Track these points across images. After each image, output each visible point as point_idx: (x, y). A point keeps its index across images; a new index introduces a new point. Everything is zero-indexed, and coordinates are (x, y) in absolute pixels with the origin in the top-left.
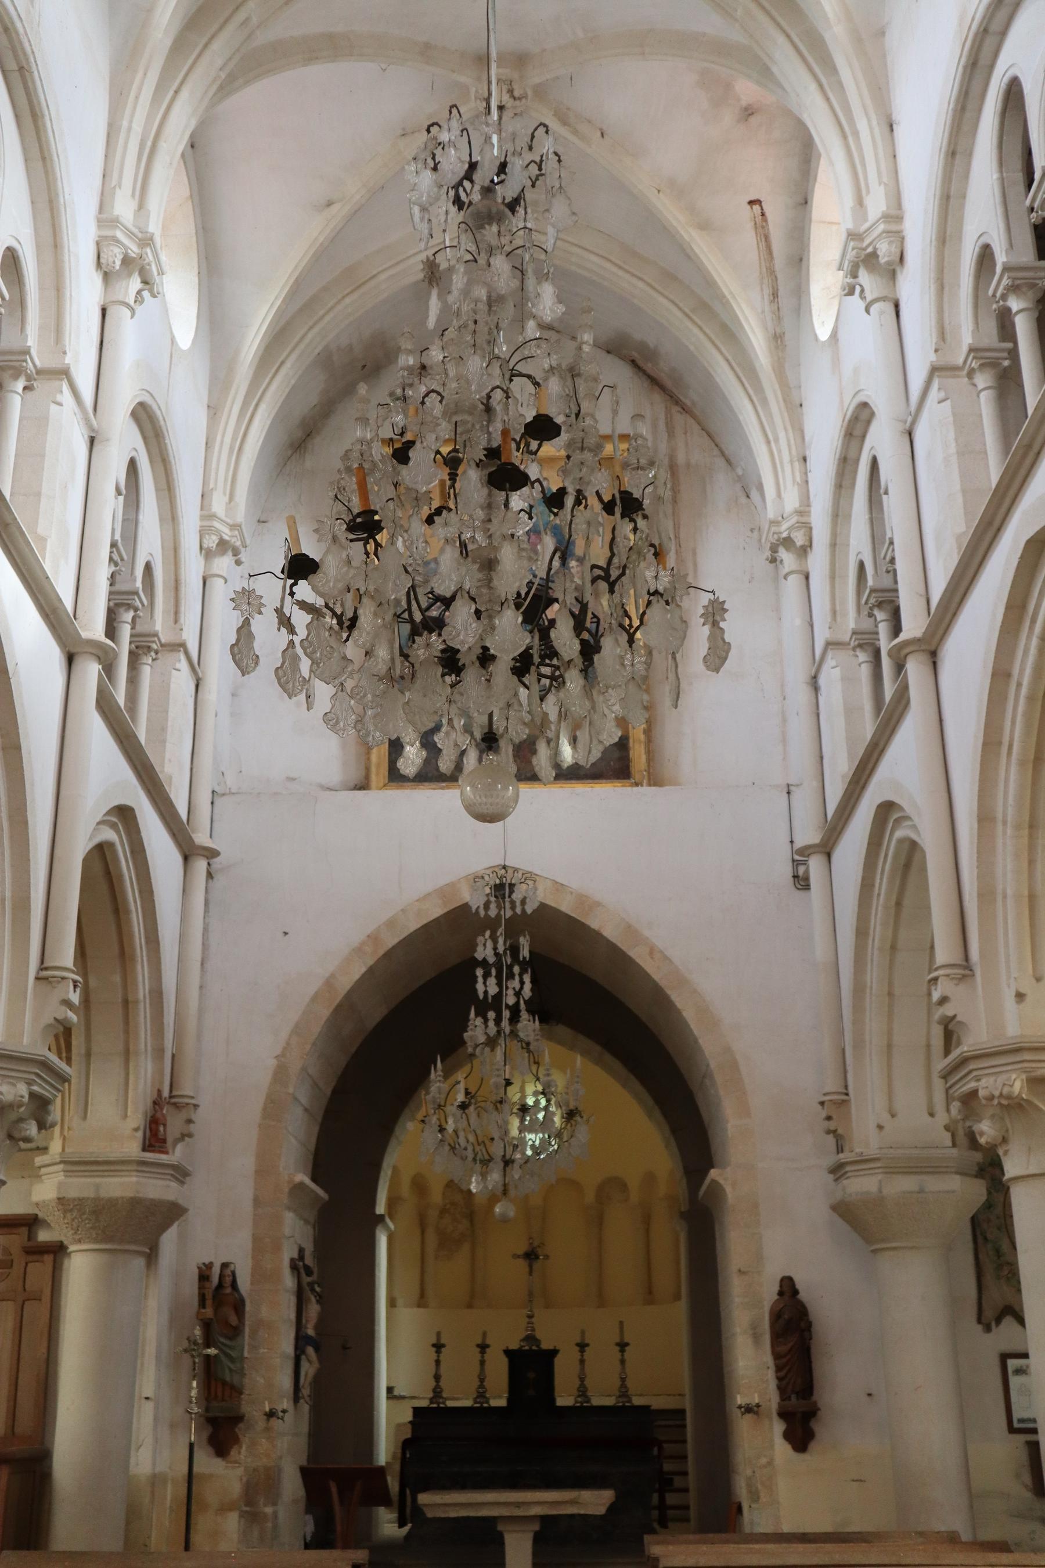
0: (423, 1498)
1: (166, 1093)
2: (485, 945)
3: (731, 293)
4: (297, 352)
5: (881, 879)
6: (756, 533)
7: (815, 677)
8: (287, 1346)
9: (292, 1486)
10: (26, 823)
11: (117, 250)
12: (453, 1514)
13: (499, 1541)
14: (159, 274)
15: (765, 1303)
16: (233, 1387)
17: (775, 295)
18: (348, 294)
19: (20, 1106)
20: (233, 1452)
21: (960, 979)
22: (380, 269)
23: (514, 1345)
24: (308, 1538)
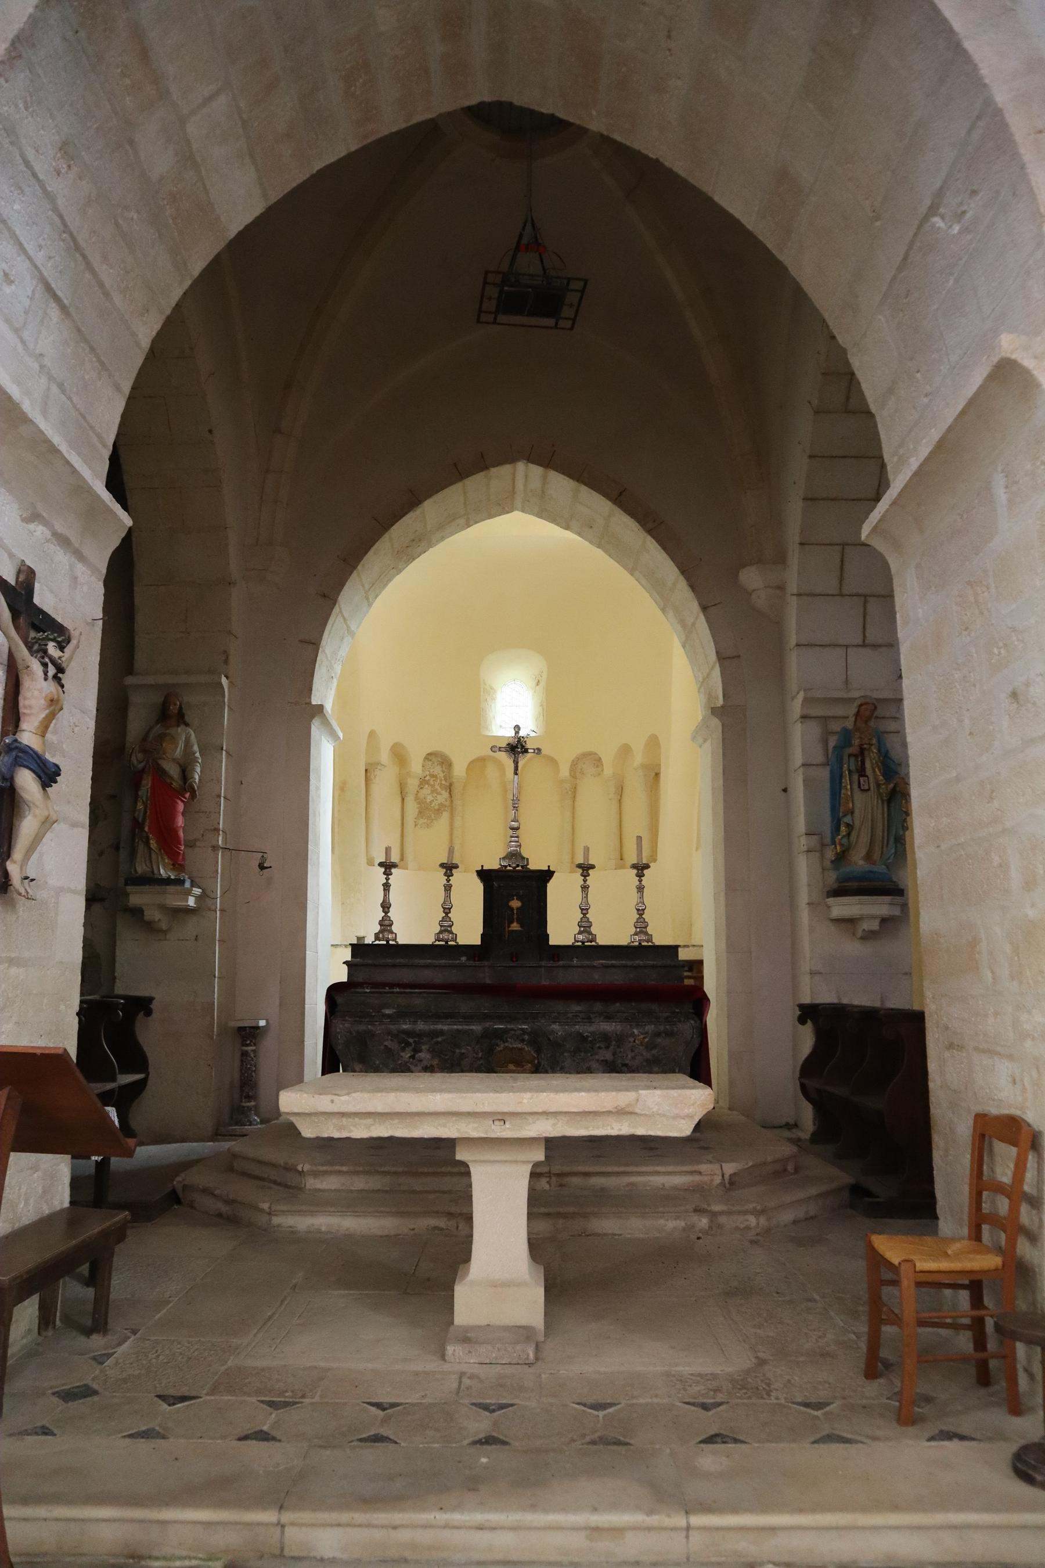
23: (493, 864)
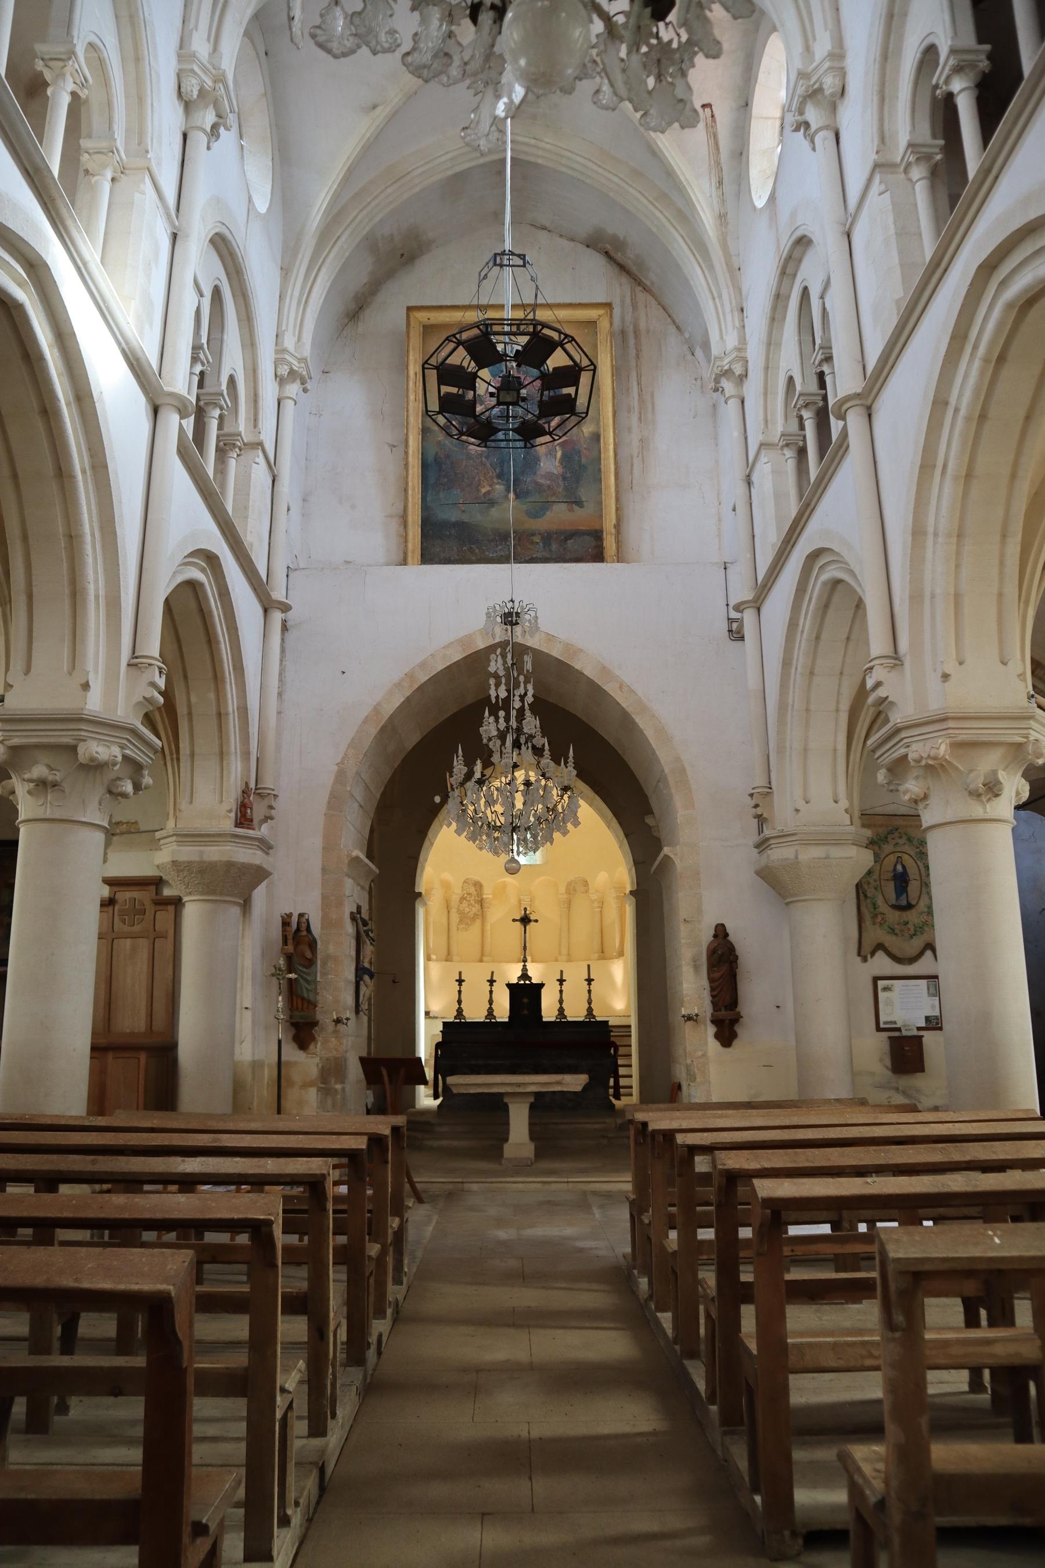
0: (450, 1080)
1: (252, 785)
2: (496, 661)
3: (687, 180)
4: (350, 229)
5: (805, 618)
6: (699, 381)
7: (749, 476)
8: (350, 973)
9: (355, 1071)
10: (115, 533)
11: (194, 81)
12: (472, 1091)
13: (505, 1109)
14: (231, 112)
15: (703, 943)
16: (309, 1002)
17: (720, 183)
18: (389, 186)
19: (114, 764)
20: (312, 1047)
21: (892, 667)
22: (414, 167)
24: (369, 1107)
